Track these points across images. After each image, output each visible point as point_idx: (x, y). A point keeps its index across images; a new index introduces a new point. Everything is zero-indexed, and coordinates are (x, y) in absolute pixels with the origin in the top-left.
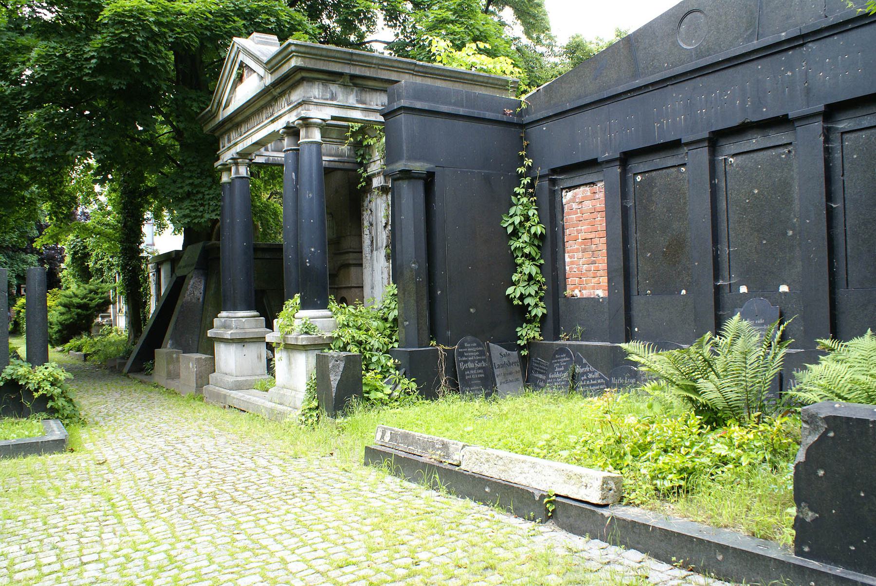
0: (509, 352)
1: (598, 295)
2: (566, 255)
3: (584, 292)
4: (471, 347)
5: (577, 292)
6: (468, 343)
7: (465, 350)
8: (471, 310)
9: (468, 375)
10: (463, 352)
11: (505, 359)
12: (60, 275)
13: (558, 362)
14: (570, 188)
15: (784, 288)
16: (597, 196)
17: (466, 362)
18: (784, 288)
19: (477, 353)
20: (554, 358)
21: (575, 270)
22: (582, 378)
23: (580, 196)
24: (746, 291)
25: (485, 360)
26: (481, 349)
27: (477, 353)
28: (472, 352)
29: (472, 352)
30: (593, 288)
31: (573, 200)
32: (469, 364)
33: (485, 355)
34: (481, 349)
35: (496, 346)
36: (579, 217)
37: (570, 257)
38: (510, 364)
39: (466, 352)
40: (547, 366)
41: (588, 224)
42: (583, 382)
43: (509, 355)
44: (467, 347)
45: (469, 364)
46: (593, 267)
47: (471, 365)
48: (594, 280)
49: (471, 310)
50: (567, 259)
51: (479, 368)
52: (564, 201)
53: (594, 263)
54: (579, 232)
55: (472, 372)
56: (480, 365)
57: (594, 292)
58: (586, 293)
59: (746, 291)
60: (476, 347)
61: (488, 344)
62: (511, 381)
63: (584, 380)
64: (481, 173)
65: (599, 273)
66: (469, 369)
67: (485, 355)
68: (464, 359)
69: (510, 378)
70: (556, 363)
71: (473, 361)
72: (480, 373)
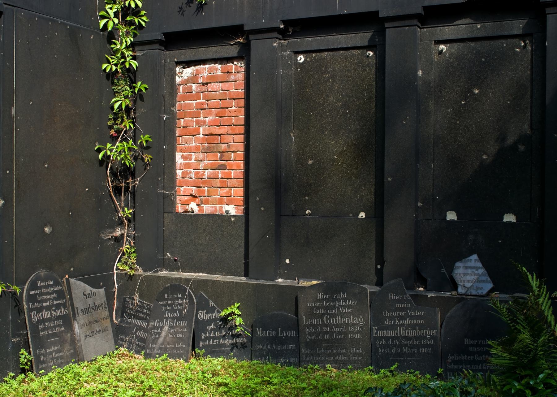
1: (227, 212)
2: (179, 155)
3: (205, 206)
4: (46, 287)
6: (42, 281)
7: (38, 291)
8: (46, 229)
9: (43, 330)
10: (36, 295)
11: (90, 301)
12: (243, 170)
13: (169, 305)
14: (188, 64)
15: (510, 218)
17: (39, 310)
18: (510, 218)
19: (55, 296)
20: (161, 298)
22: (209, 328)
23: (205, 75)
24: (455, 218)
25: (64, 305)
26: (59, 288)
27: (55, 296)
30: (221, 202)
31: (194, 79)
32: (44, 312)
33: (64, 298)
34: (59, 288)
35: (79, 282)
36: (202, 104)
37: (184, 158)
38: (95, 307)
39: (41, 294)
40: (149, 309)
41: (217, 115)
42: (210, 333)
44: (40, 288)
45: (44, 312)
46: (220, 173)
47: (46, 314)
48: (220, 191)
49: (46, 229)
50: (179, 159)
51: (58, 318)
52: (178, 80)
53: (222, 167)
54: (200, 124)
55: (48, 324)
56: (58, 314)
57: (221, 209)
58: (207, 209)
59: (455, 218)
60: (51, 286)
61: (68, 280)
62: (99, 332)
63: (212, 330)
64: (66, 25)
66: (44, 321)
67: (64, 298)
68: (37, 305)
69: (97, 327)
70: (165, 305)
71: (49, 308)
72: (59, 326)
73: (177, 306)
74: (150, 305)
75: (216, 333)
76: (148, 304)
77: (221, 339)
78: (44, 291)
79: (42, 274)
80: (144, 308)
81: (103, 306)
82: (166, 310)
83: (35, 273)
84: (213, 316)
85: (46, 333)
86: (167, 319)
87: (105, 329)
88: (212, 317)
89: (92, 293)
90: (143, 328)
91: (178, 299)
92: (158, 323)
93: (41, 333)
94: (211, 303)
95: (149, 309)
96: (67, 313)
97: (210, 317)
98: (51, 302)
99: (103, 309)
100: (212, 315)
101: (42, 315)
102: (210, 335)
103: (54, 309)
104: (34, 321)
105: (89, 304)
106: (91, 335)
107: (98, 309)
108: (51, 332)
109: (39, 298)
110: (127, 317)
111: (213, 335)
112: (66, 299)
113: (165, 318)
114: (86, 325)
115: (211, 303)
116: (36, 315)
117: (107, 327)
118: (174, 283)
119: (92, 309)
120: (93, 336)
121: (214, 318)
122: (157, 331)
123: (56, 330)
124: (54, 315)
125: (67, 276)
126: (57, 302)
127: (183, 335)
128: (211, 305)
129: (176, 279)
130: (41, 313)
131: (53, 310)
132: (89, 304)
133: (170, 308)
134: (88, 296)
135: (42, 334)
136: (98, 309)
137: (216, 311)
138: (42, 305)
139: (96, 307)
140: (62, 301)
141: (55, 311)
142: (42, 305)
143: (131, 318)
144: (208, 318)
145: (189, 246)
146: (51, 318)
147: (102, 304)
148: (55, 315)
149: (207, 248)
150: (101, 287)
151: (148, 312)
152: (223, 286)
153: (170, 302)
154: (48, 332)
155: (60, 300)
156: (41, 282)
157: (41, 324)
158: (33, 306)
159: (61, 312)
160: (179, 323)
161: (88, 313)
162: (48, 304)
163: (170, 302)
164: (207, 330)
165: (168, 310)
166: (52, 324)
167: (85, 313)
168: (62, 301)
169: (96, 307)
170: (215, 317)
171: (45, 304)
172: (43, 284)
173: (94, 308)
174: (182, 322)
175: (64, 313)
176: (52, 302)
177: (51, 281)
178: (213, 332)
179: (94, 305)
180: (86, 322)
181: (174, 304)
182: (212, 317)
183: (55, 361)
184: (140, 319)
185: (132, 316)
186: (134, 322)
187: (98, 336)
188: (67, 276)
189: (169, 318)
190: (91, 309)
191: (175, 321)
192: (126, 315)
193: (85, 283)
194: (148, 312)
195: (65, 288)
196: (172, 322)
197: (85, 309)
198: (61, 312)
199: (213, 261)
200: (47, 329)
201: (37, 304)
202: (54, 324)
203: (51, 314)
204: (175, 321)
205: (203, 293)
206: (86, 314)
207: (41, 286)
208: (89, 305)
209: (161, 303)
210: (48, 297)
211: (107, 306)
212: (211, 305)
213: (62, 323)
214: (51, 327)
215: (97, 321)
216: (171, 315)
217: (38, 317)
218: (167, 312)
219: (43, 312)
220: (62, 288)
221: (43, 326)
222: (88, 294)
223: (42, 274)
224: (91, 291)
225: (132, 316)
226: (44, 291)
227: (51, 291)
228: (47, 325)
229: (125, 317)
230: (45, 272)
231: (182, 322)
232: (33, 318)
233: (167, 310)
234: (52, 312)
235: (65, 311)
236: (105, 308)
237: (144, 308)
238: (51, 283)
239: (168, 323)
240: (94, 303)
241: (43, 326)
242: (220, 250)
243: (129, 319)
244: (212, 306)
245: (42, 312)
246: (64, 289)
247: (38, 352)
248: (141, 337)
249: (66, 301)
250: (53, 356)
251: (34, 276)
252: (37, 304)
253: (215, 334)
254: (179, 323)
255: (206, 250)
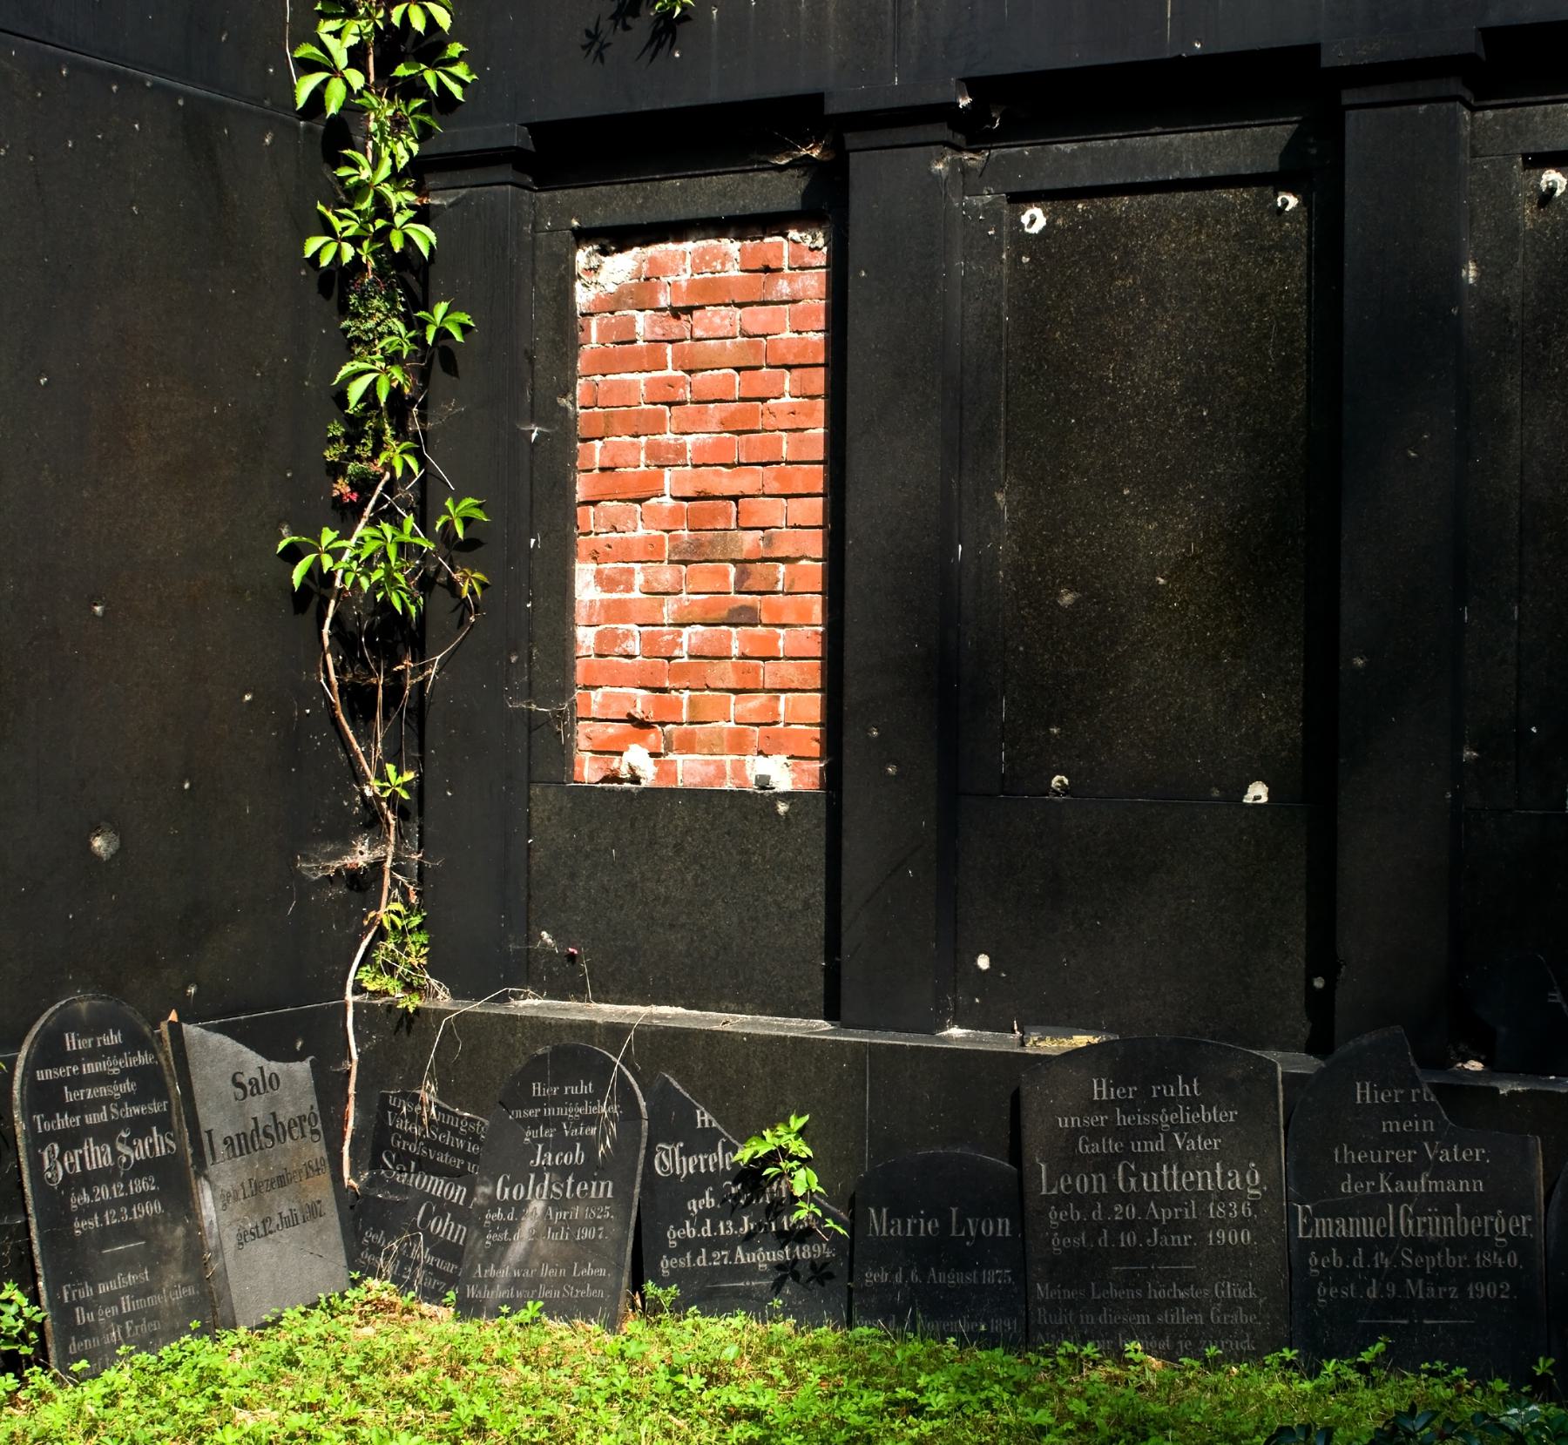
0: (274, 1066)
1: (763, 782)
4: (94, 1054)
5: (637, 759)
6: (82, 1035)
8: (98, 843)
9: (86, 1212)
11: (257, 1107)
13: (547, 1122)
16: (783, 288)
17: (70, 1140)
19: (128, 1086)
20: (517, 1096)
21: (635, 647)
22: (694, 1206)
23: (684, 278)
26: (143, 1059)
27: (128, 1086)
28: (103, 1079)
29: (103, 1079)
30: (738, 744)
31: (640, 293)
33: (162, 1093)
34: (143, 1059)
35: (216, 1039)
36: (671, 383)
38: (277, 1131)
39: (78, 1082)
40: (475, 1139)
43: (274, 1081)
44: (77, 1058)
46: (736, 641)
47: (97, 1156)
49: (98, 843)
50: (586, 586)
52: (583, 297)
53: (743, 618)
54: (662, 459)
55: (103, 1192)
56: (140, 1152)
57: (739, 769)
58: (689, 770)
60: (116, 1051)
61: (175, 1029)
62: (290, 1222)
63: (704, 1214)
64: (174, 94)
65: (769, 674)
66: (88, 1180)
67: (162, 1093)
68: (64, 1122)
69: (283, 1204)
70: (533, 1124)
71: (105, 1134)
72: (143, 1197)
73: (577, 1125)
74: (476, 1121)
75: (721, 1224)
76: (469, 1119)
77: (739, 1249)
78: (89, 1068)
79: (83, 1006)
80: (455, 1132)
81: (306, 1124)
82: (535, 1141)
83: (57, 1006)
84: (711, 1163)
85: (94, 1223)
86: (540, 1173)
87: (313, 1212)
88: (707, 1165)
89: (267, 1075)
90: (453, 1207)
91: (579, 1100)
92: (507, 1190)
93: (77, 1224)
94: (702, 1115)
95: (475, 1139)
96: (172, 1149)
97: (697, 1167)
98: (113, 1110)
99: (304, 1136)
100: (706, 1161)
101: (82, 1157)
102: (699, 1231)
103: (125, 1135)
104: (50, 1180)
105: (255, 1119)
106: (262, 1232)
107: (288, 1138)
108: (114, 1222)
109: (69, 1096)
110: (394, 1166)
111: (704, 1264)
112: (168, 1098)
113: (532, 1170)
114: (241, 1196)
115: (702, 1115)
116: (61, 1159)
117: (319, 1202)
118: (568, 1040)
119: (267, 1135)
120: (270, 1236)
121: (712, 1169)
122: (505, 1216)
123: (130, 1214)
124: (124, 1160)
125: (173, 1016)
126: (137, 1111)
127: (598, 1232)
128: (703, 1122)
129: (574, 1027)
130: (76, 1152)
131: (122, 1140)
132: (255, 1119)
133: (550, 1134)
134: (249, 1088)
135: (79, 1227)
136: (288, 1138)
137: (720, 1144)
138: (82, 1120)
139: (280, 1130)
140: (155, 1108)
141: (129, 1143)
142: (82, 1120)
143: (408, 1171)
144: (692, 1171)
145: (622, 907)
146: (115, 1168)
147: (302, 1118)
148: (128, 1157)
149: (689, 914)
150: (299, 1057)
151: (471, 1148)
152: (748, 1055)
153: (549, 1112)
154: (102, 1220)
155: (146, 1102)
156: (76, 1038)
157: (78, 1193)
158: (48, 1127)
159: (152, 1146)
160: (586, 1188)
161: (248, 1152)
162: (101, 1117)
163: (549, 1112)
164: (687, 1214)
165: (545, 1140)
166: (118, 1190)
167: (238, 1152)
168: (155, 1108)
169: (280, 1130)
170: (716, 1165)
171: (91, 1119)
172: (85, 1043)
173: (272, 1131)
174: (594, 1184)
175: (160, 1151)
176: (119, 1109)
177: (115, 1033)
178: (708, 1221)
179: (271, 1123)
180: (242, 1185)
181: (564, 1118)
182: (707, 1165)
183: (128, 1329)
184: (439, 1175)
185: (413, 1164)
186: (420, 1185)
187: (285, 1235)
188: (173, 1016)
189: (550, 1169)
190: (262, 1138)
191: (570, 1181)
192: (390, 1159)
193: (238, 1041)
194: (471, 1148)
195: (167, 1059)
196: (558, 1186)
197: (238, 1135)
198: (152, 1146)
199: (708, 960)
200: (100, 1208)
201: (62, 1117)
202: (126, 1189)
203: (115, 1154)
204: (570, 1181)
205: (671, 1080)
206: (242, 1154)
207: (78, 1050)
208: (252, 1122)
209: (519, 1114)
210: (103, 1091)
211: (319, 1126)
212: (703, 1122)
213: (153, 1188)
214: (114, 1203)
215: (282, 1181)
216: (553, 1159)
217: (66, 1164)
218: (540, 1147)
219: (86, 1147)
220: (156, 1058)
221: (86, 1199)
222: (250, 1083)
223: (83, 1006)
224: (261, 1068)
225: (413, 1164)
226: (89, 1068)
227: (115, 1071)
228: (100, 1195)
229: (386, 1167)
230: (93, 998)
231: (594, 1184)
232: (49, 1170)
233: (539, 1140)
234: (119, 1147)
235: (166, 1145)
236: (314, 1132)
237: (455, 1132)
238: (113, 1039)
239: (542, 1187)
240: (274, 1114)
241: (86, 1199)
242: (735, 919)
243: (401, 1172)
244: (707, 1125)
245: (81, 1147)
246: (164, 1063)
247: (66, 1294)
248: (445, 1241)
249: (169, 1106)
250: (120, 1309)
251: (53, 1014)
252: (62, 1117)
253: (715, 1228)
254: (586, 1188)
255: (683, 919)
